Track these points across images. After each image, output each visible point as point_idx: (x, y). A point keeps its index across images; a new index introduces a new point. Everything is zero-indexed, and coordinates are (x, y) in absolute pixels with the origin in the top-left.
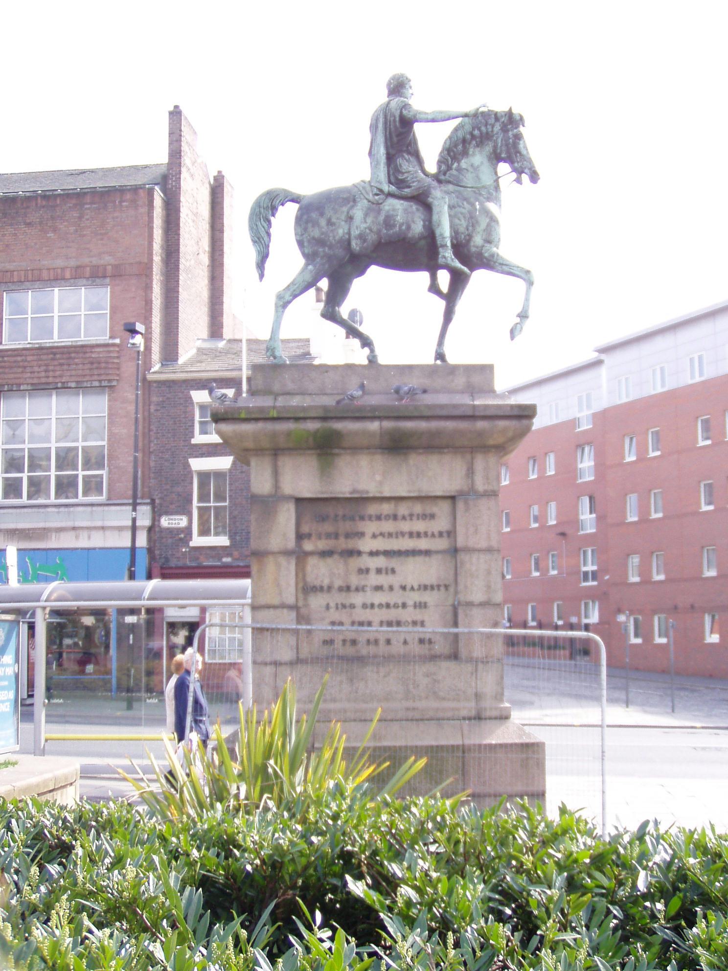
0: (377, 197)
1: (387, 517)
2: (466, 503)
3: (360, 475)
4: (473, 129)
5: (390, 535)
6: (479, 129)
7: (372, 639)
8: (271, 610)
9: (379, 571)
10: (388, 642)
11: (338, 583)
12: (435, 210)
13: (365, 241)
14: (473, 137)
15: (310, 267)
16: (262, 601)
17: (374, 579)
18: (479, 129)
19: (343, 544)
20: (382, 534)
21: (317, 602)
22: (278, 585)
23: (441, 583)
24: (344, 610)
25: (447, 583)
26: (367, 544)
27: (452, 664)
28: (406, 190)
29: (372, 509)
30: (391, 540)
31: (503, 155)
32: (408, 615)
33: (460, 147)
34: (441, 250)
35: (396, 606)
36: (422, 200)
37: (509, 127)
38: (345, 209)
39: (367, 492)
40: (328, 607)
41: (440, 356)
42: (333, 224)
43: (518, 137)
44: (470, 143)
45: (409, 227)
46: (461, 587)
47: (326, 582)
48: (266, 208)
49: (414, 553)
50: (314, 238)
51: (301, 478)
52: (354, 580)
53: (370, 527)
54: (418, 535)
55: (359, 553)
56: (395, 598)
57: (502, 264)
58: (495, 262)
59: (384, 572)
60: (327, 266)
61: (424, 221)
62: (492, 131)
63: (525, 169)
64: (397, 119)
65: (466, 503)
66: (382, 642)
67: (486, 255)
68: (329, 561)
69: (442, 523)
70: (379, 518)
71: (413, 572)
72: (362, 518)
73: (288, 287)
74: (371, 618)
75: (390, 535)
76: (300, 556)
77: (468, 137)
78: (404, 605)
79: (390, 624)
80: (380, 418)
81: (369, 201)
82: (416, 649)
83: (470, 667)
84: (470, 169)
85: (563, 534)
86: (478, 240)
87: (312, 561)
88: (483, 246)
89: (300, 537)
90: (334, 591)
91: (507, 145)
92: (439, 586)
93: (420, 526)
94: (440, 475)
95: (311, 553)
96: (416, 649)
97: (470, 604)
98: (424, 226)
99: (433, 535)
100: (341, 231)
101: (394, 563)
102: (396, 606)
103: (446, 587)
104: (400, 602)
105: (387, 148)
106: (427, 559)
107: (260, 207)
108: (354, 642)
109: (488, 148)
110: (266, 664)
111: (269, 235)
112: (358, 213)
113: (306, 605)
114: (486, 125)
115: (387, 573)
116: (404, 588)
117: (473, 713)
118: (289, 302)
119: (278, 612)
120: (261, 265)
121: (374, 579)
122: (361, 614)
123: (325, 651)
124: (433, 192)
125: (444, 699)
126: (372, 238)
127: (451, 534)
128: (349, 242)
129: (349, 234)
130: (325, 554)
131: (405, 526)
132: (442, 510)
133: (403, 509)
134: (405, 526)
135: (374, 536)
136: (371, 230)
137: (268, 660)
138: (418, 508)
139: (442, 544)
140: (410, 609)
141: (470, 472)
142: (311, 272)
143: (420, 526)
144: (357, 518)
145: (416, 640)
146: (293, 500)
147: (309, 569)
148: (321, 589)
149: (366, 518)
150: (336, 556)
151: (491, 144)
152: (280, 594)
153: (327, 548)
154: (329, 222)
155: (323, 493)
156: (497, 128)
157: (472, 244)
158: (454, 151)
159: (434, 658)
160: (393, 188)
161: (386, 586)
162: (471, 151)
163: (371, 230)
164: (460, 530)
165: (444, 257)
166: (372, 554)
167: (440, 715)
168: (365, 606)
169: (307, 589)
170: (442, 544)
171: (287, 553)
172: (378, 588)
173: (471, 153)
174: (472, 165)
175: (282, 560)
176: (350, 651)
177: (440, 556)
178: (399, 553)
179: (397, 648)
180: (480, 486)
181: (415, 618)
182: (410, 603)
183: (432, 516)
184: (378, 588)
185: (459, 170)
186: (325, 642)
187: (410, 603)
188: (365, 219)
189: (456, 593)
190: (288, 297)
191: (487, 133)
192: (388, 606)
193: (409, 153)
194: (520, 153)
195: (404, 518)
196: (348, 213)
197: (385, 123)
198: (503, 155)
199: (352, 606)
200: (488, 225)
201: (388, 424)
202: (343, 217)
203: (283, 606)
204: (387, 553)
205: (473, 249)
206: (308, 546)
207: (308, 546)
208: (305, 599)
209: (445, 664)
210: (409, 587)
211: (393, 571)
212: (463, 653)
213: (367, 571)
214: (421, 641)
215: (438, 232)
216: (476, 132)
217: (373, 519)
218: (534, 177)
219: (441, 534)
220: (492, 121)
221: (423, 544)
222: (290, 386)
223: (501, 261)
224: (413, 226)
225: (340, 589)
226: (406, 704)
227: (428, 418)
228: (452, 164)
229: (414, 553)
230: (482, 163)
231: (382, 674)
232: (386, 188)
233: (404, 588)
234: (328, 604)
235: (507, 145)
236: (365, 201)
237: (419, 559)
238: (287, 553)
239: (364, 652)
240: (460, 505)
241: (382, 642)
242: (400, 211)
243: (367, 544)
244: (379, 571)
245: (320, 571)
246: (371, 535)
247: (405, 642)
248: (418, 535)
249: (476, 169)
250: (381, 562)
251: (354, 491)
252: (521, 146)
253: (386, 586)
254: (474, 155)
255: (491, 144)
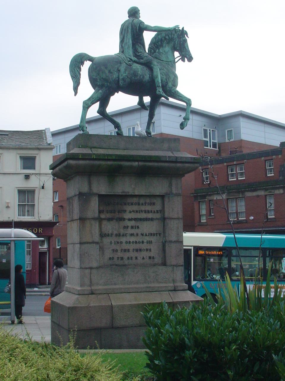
0: (129, 62)
1: (136, 204)
2: (169, 198)
3: (125, 186)
4: (166, 35)
5: (137, 212)
6: (168, 36)
7: (130, 257)
8: (88, 244)
9: (132, 227)
10: (136, 258)
11: (115, 232)
12: (155, 70)
13: (125, 81)
14: (165, 39)
15: (100, 91)
16: (84, 240)
17: (130, 231)
18: (168, 36)
19: (117, 215)
20: (133, 211)
21: (106, 240)
22: (91, 233)
23: (157, 233)
24: (118, 244)
25: (160, 232)
26: (127, 216)
27: (164, 267)
28: (141, 60)
29: (130, 200)
30: (137, 214)
31: (178, 48)
32: (144, 246)
33: (160, 43)
34: (157, 88)
35: (139, 242)
36: (148, 65)
37: (181, 36)
38: (116, 66)
39: (129, 193)
40: (111, 243)
41: (148, 133)
42: (111, 73)
43: (185, 41)
44: (164, 42)
45: (144, 77)
46: (167, 235)
47: (110, 232)
48: (79, 63)
49: (147, 219)
50: (103, 78)
51: (101, 187)
52: (122, 231)
53: (129, 208)
54: (148, 212)
55: (124, 219)
56: (140, 239)
57: (179, 96)
58: (176, 95)
59: (134, 227)
60: (108, 91)
61: (149, 75)
62: (174, 37)
63: (186, 56)
64: (138, 28)
65: (169, 198)
66: (134, 258)
67: (173, 91)
68: (112, 222)
69: (158, 207)
70: (132, 204)
71: (147, 228)
72: (125, 204)
73: (89, 99)
74: (129, 248)
75: (137, 212)
76: (100, 220)
77: (163, 39)
78: (143, 242)
79: (137, 250)
80: (138, 161)
81: (127, 64)
82: (147, 261)
83: (170, 268)
84: (163, 53)
85: (62, 206)
86: (170, 85)
87: (104, 222)
88: (172, 87)
89: (100, 212)
90: (114, 236)
91: (180, 44)
92: (157, 234)
93: (149, 208)
94: (158, 187)
95: (105, 219)
96: (147, 261)
97: (171, 242)
98: (149, 77)
99: (154, 212)
100: (115, 76)
101: (138, 224)
102: (139, 242)
103: (160, 234)
104: (141, 241)
105: (132, 41)
106: (152, 222)
107: (76, 62)
108: (122, 258)
109: (172, 44)
110: (86, 268)
111: (80, 74)
112: (122, 69)
113: (102, 242)
114: (171, 35)
115: (135, 228)
116: (142, 235)
117: (173, 288)
118: (90, 106)
119: (92, 245)
120: (76, 89)
121: (130, 231)
122: (125, 246)
123: (110, 262)
124: (153, 62)
125: (161, 282)
126: (128, 80)
127: (162, 211)
128: (118, 81)
129: (118, 77)
130: (109, 220)
131: (143, 208)
132: (158, 202)
133: (142, 201)
134: (143, 208)
135: (130, 212)
136: (128, 77)
137: (87, 267)
138: (148, 201)
139: (158, 216)
140: (145, 244)
141: (170, 185)
142: (101, 93)
143: (149, 208)
144: (123, 204)
145: (148, 257)
146: (98, 195)
147: (103, 226)
148: (108, 235)
149: (127, 204)
150: (114, 220)
151: (173, 43)
152: (92, 236)
153: (111, 217)
154: (110, 72)
155: (110, 193)
156: (176, 36)
157: (168, 86)
158: (156, 44)
159: (154, 265)
160: (135, 59)
161: (135, 234)
162: (164, 45)
163: (128, 77)
164: (166, 210)
165: (159, 91)
166: (130, 220)
167: (160, 289)
168: (126, 242)
169: (102, 235)
170: (158, 216)
171: (94, 219)
172: (132, 235)
173: (164, 46)
174: (165, 51)
175: (93, 222)
176: (120, 262)
177: (157, 221)
178: (140, 219)
179: (140, 261)
180: (174, 191)
181: (147, 248)
182: (145, 241)
183: (154, 204)
184: (132, 235)
185: (159, 53)
186: (110, 258)
187: (145, 241)
188: (125, 72)
189: (164, 236)
190: (89, 103)
191: (172, 38)
192: (136, 242)
193: (141, 44)
194: (185, 48)
195: (142, 204)
196: (118, 68)
197: (132, 29)
198: (178, 48)
199: (121, 243)
200: (174, 78)
201: (141, 163)
202: (116, 70)
203: (93, 243)
204: (135, 219)
205: (168, 89)
206: (103, 216)
207: (103, 216)
208: (101, 240)
209: (161, 267)
210: (145, 234)
211: (138, 227)
212: (168, 262)
213: (128, 227)
214: (150, 258)
215: (156, 81)
216: (167, 37)
217: (130, 204)
218: (190, 59)
219: (157, 212)
220: (174, 32)
221: (150, 216)
222: (96, 145)
223: (178, 95)
224: (145, 77)
225: (116, 235)
226: (145, 285)
227: (154, 161)
228: (156, 50)
229: (147, 219)
230: (169, 51)
231: (135, 272)
232: (134, 59)
233: (142, 235)
234: (111, 242)
235: (180, 44)
236: (125, 64)
237: (148, 222)
238: (94, 219)
239: (126, 262)
240: (166, 199)
241: (134, 258)
242: (140, 69)
243: (127, 216)
244: (132, 227)
245: (109, 227)
246: (129, 211)
247: (143, 258)
248: (148, 212)
249: (166, 53)
250: (133, 223)
251: (123, 192)
252: (186, 45)
253: (135, 234)
254: (165, 47)
255: (173, 43)
